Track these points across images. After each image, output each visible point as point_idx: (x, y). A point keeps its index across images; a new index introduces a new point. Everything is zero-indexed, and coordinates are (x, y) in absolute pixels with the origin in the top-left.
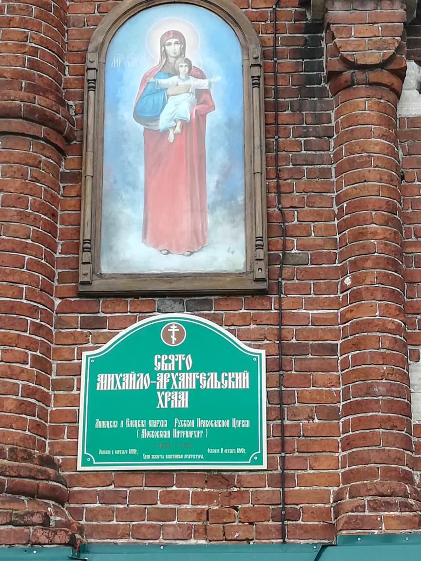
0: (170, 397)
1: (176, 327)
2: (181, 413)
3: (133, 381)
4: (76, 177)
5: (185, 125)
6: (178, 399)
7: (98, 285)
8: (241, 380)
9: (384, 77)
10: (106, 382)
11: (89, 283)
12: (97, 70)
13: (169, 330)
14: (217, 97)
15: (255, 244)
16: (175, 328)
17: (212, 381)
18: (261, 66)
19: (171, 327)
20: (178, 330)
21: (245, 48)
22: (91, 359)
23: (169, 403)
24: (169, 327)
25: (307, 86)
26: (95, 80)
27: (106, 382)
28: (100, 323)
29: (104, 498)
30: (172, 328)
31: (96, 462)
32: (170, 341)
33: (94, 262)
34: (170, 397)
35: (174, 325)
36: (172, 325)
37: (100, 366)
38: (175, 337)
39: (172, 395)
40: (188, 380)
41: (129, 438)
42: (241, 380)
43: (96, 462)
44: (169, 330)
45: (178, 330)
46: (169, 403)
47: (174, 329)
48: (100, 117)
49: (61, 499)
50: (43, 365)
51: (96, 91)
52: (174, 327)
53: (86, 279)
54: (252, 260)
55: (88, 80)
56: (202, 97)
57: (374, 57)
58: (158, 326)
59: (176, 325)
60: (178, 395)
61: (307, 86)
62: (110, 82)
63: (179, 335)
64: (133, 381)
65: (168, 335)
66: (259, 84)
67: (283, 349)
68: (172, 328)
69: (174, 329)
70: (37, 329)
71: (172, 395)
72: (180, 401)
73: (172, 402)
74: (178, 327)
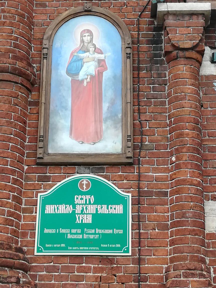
0: (83, 217)
1: (86, 181)
2: (88, 226)
3: (64, 209)
4: (37, 104)
5: (92, 77)
6: (87, 219)
7: (47, 159)
8: (119, 209)
9: (194, 54)
10: (50, 209)
11: (42, 158)
12: (48, 49)
13: (83, 183)
14: (108, 63)
15: (127, 139)
16: (86, 182)
17: (104, 210)
18: (131, 48)
19: (84, 181)
20: (87, 183)
21: (123, 39)
22: (42, 197)
23: (82, 220)
24: (82, 181)
25: (154, 59)
26: (47, 54)
27: (50, 209)
28: (47, 179)
29: (48, 269)
30: (84, 182)
31: (44, 250)
32: (83, 188)
33: (45, 147)
34: (83, 217)
35: (85, 180)
36: (84, 180)
37: (47, 201)
38: (86, 186)
39: (83, 216)
40: (92, 209)
41: (60, 238)
42: (119, 209)
43: (44, 250)
44: (83, 183)
45: (87, 183)
46: (82, 220)
47: (85, 182)
48: (49, 73)
49: (26, 270)
50: (18, 200)
51: (47, 59)
52: (85, 181)
53: (41, 156)
54: (125, 147)
55: (44, 54)
56: (101, 63)
57: (188, 44)
58: (77, 181)
59: (86, 180)
60: (87, 216)
61: (154, 59)
62: (54, 55)
63: (88, 185)
64: (64, 209)
65: (82, 185)
66: (130, 57)
67: (140, 193)
68: (84, 182)
69: (85, 182)
70: (15, 181)
71: (83, 216)
72: (87, 220)
73: (84, 220)
74: (87, 181)
